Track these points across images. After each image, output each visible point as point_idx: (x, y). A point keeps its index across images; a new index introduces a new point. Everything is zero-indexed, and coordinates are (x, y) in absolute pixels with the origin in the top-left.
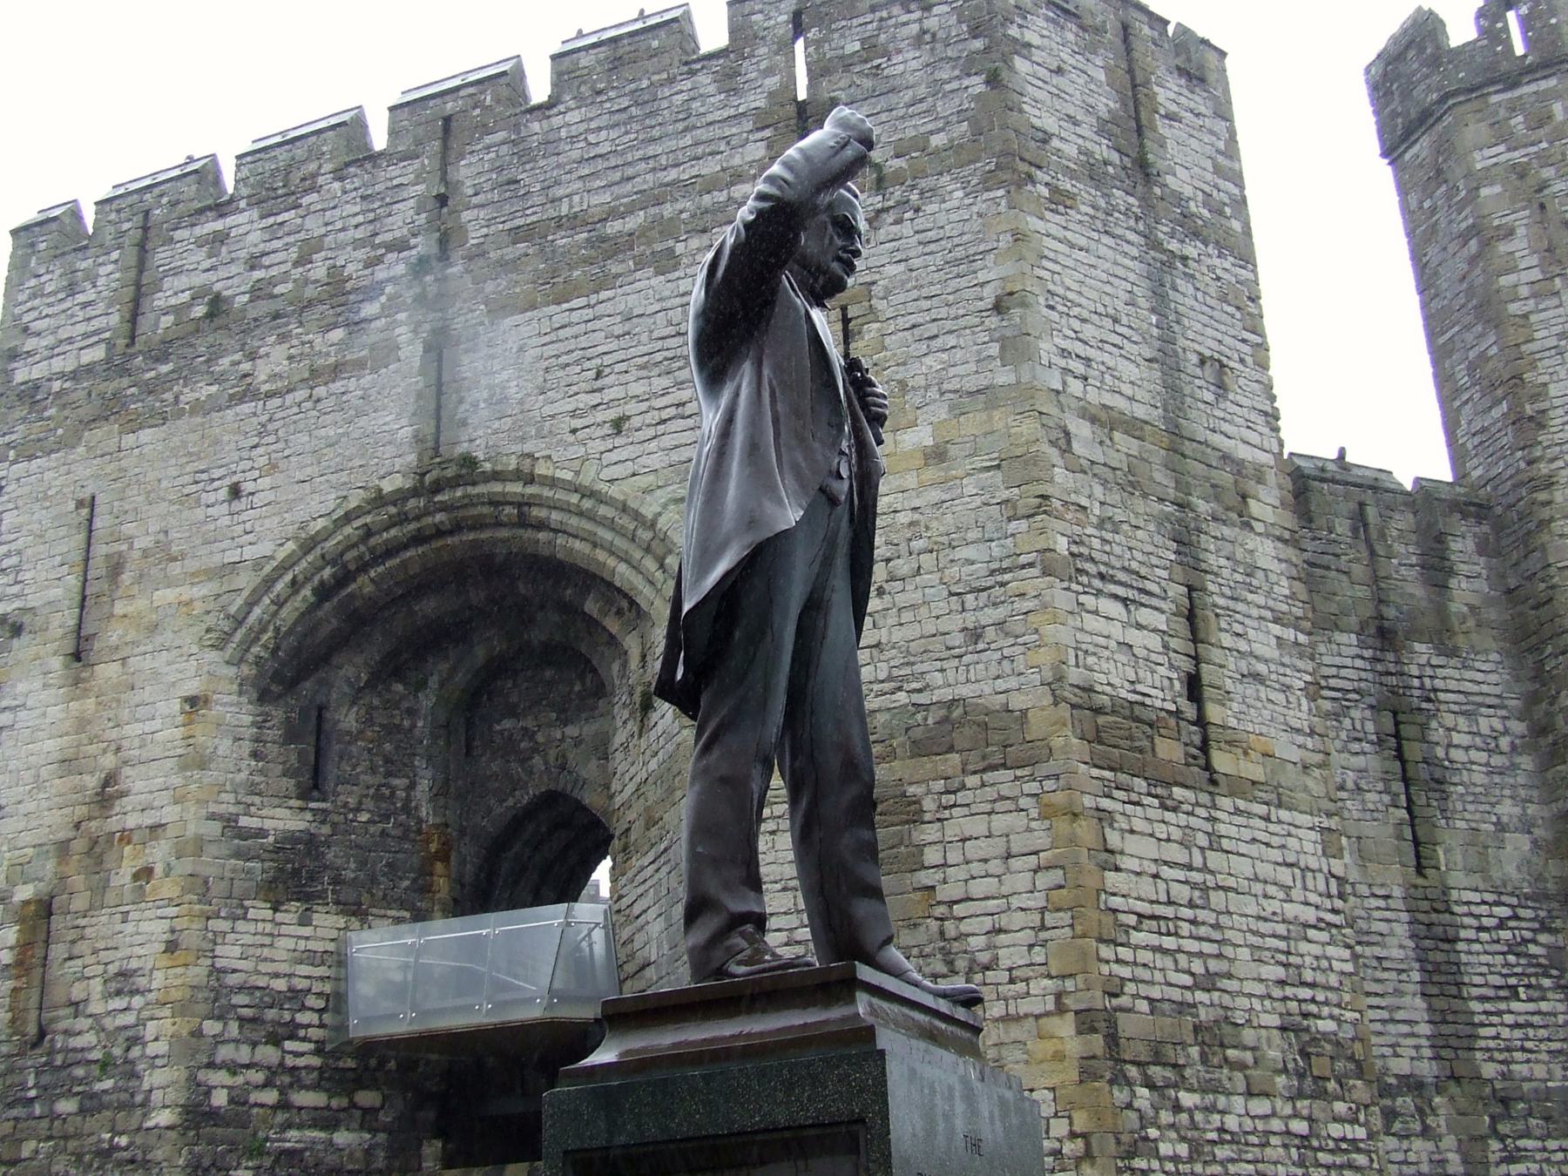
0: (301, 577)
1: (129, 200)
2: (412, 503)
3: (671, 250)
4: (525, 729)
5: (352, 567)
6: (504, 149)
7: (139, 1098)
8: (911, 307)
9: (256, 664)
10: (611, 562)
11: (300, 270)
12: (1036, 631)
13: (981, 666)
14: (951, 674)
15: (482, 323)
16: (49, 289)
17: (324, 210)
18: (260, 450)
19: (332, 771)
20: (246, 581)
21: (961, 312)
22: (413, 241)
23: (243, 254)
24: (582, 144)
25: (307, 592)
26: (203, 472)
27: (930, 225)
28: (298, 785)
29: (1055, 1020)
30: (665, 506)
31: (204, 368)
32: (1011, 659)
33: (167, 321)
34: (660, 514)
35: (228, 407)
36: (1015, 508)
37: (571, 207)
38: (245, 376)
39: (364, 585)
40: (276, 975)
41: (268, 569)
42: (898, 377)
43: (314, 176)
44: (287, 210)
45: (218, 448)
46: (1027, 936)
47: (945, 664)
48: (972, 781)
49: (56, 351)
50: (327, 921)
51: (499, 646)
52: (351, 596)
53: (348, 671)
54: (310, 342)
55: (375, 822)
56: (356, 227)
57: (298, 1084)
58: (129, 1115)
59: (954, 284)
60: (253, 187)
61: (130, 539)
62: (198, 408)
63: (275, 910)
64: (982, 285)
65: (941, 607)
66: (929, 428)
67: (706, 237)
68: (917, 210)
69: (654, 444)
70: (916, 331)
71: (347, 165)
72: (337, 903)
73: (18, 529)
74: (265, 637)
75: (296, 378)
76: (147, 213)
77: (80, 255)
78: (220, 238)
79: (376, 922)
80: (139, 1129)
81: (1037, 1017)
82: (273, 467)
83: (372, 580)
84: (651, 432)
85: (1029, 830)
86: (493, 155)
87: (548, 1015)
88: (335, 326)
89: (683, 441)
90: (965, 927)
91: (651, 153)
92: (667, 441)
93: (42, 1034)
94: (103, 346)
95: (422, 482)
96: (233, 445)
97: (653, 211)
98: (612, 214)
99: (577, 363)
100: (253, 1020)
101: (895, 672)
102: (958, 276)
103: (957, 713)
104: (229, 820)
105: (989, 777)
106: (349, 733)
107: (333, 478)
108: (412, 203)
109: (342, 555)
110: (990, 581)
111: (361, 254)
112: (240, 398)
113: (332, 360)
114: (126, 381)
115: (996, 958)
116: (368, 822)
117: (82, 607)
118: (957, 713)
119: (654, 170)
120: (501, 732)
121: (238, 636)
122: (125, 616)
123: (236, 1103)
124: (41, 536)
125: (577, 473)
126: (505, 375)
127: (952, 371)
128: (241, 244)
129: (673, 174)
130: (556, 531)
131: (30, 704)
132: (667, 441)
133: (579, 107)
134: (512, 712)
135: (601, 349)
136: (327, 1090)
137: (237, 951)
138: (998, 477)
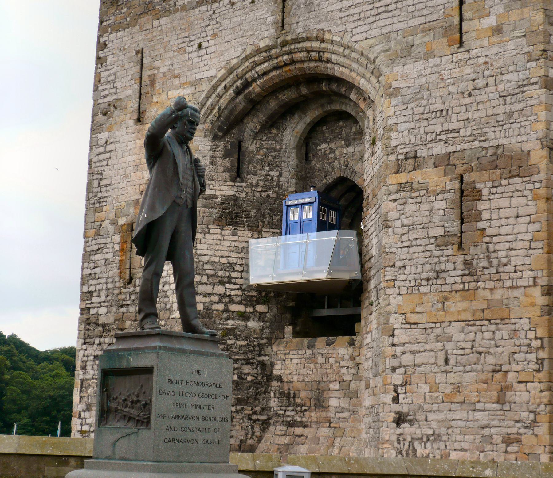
0: (228, 85)
2: (273, 51)
4: (331, 149)
7: (168, 306)
9: (211, 124)
10: (358, 78)
14: (498, 133)
19: (244, 169)
20: (205, 87)
25: (231, 91)
26: (187, 37)
28: (231, 176)
30: (379, 54)
32: (525, 127)
34: (377, 57)
35: (196, 7)
39: (255, 88)
40: (223, 257)
41: (214, 82)
46: (523, 252)
47: (496, 129)
48: (504, 182)
52: (250, 92)
53: (251, 125)
55: (264, 191)
57: (232, 302)
58: (165, 313)
61: (158, 68)
63: (222, 229)
65: (495, 103)
66: (495, 17)
69: (375, 24)
72: (248, 226)
74: (214, 111)
80: (169, 318)
81: (525, 287)
84: (373, 19)
85: (527, 205)
87: (329, 277)
89: (388, 23)
90: (497, 247)
92: (381, 23)
95: (276, 42)
96: (198, 26)
100: (213, 276)
101: (474, 132)
103: (500, 151)
105: (512, 181)
106: (253, 152)
107: (240, 40)
109: (245, 74)
110: (517, 91)
116: (261, 191)
117: (140, 98)
118: (500, 151)
120: (321, 150)
122: (157, 102)
125: (342, 38)
130: (335, 64)
132: (381, 23)
134: (325, 141)
136: (244, 305)
137: (206, 247)
138: (523, 41)
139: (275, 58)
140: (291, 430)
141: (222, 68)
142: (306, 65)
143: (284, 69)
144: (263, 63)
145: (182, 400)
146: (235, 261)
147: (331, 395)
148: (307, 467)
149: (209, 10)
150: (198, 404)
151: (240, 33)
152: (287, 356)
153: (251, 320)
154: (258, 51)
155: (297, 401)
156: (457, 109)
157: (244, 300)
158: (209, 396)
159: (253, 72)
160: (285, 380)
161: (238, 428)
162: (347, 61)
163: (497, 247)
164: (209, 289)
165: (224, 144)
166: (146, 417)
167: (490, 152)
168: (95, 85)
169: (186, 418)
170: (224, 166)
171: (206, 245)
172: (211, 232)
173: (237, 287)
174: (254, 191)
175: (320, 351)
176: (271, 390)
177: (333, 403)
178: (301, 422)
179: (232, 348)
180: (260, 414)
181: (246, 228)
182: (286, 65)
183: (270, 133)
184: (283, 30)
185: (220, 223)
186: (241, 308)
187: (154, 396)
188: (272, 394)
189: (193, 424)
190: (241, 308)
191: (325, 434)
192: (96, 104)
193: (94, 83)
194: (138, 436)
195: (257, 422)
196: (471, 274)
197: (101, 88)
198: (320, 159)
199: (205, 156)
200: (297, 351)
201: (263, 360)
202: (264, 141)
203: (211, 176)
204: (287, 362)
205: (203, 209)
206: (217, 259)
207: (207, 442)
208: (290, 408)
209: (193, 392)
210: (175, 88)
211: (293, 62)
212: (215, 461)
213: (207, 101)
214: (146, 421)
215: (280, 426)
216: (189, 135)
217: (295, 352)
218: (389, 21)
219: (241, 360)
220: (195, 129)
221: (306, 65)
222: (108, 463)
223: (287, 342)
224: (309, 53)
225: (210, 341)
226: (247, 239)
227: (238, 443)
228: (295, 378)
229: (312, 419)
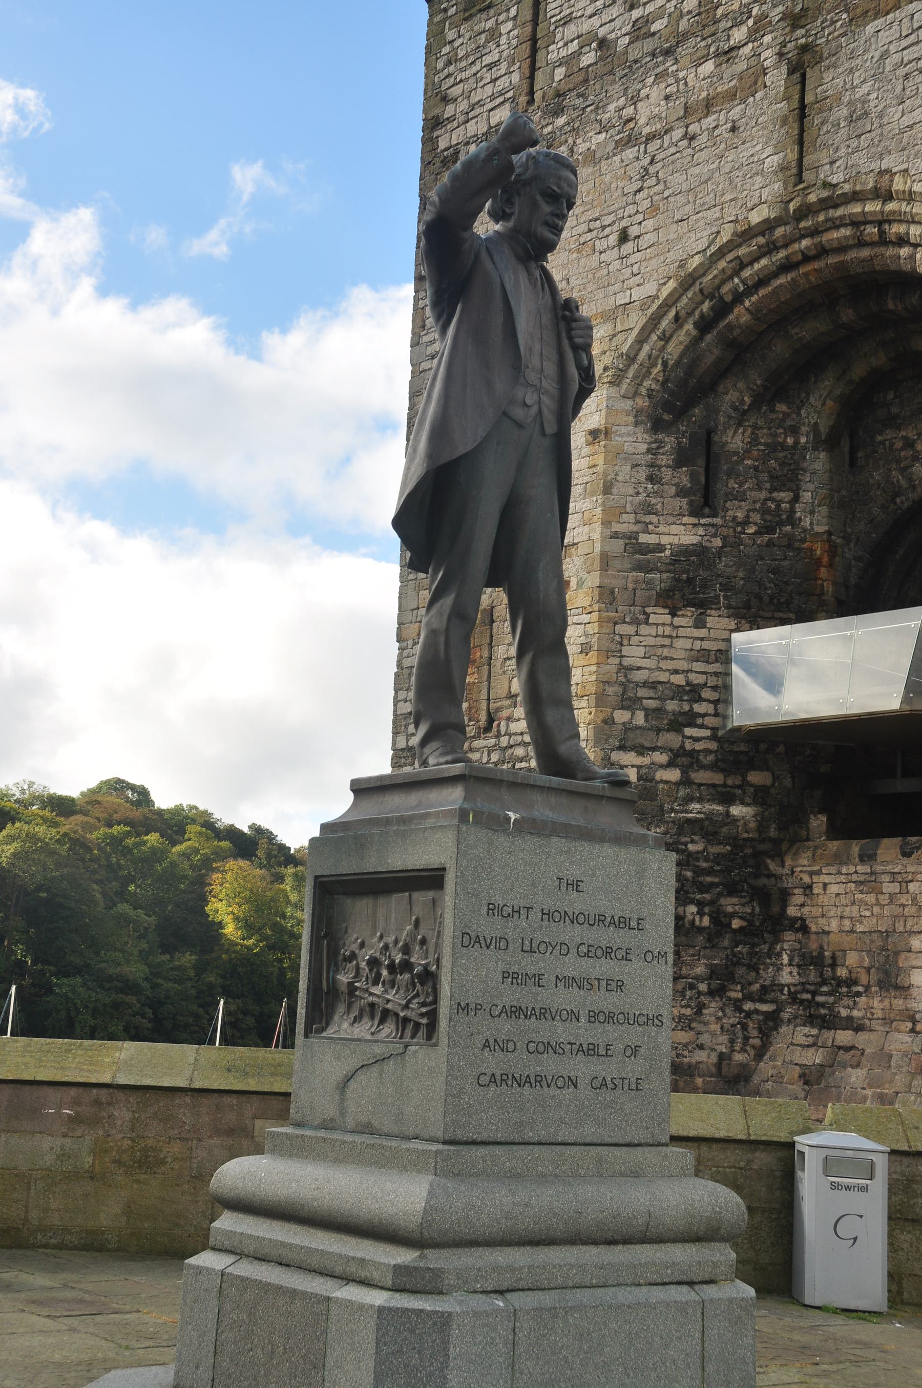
0: (683, 313)
2: (779, 231)
5: (728, 298)
9: (649, 396)
16: (461, 53)
20: (636, 321)
25: (689, 326)
26: (596, 220)
28: (691, 504)
31: (593, 116)
33: (560, 73)
35: (614, 155)
39: (740, 315)
40: (676, 672)
41: (655, 307)
49: (471, 115)
50: (717, 621)
51: (880, 360)
52: (729, 325)
53: (732, 396)
63: (673, 615)
72: (728, 607)
74: (655, 371)
77: (484, 16)
82: (654, 209)
83: (747, 309)
87: (907, 708)
88: (705, 58)
93: (491, 720)
95: (786, 210)
96: (620, 191)
100: (656, 710)
104: (630, 538)
106: (736, 453)
109: (719, 287)
116: (755, 533)
120: (882, 443)
121: (631, 373)
123: (646, 780)
126: (865, 89)
134: (893, 422)
137: (641, 651)
139: (782, 247)
140: (828, 1035)
141: (670, 278)
142: (852, 255)
143: (803, 270)
144: (757, 259)
145: (528, 964)
146: (701, 679)
147: (914, 963)
148: (876, 1137)
149: (641, 156)
150: (575, 974)
151: (707, 199)
152: (815, 879)
153: (738, 802)
154: (746, 235)
155: (839, 974)
157: (723, 761)
158: (608, 952)
159: (736, 280)
160: (814, 928)
161: (715, 1027)
165: (677, 438)
166: (424, 1010)
168: (413, 333)
169: (544, 1013)
170: (677, 485)
171: (642, 648)
172: (650, 621)
173: (708, 733)
174: (740, 533)
175: (889, 868)
176: (782, 949)
178: (850, 1018)
179: (698, 860)
180: (762, 1001)
181: (724, 611)
182: (806, 258)
183: (773, 411)
184: (801, 181)
185: (669, 602)
187: (447, 951)
188: (785, 958)
189: (561, 1032)
191: (903, 1047)
193: (413, 329)
194: (404, 1066)
195: (755, 1016)
197: (425, 339)
198: (881, 463)
199: (637, 465)
200: (836, 867)
201: (765, 886)
202: (762, 428)
203: (649, 505)
204: (816, 891)
205: (634, 573)
206: (663, 677)
207: (604, 1084)
208: (825, 989)
209: (562, 938)
211: (823, 251)
212: (628, 1139)
213: (640, 349)
214: (424, 1021)
215: (804, 1025)
216: (548, 235)
217: (833, 870)
219: (717, 885)
220: (564, 217)
221: (852, 255)
222: (325, 1140)
223: (816, 848)
224: (858, 228)
225: (610, 799)
226: (725, 635)
227: (714, 1058)
228: (834, 925)
229: (872, 1014)
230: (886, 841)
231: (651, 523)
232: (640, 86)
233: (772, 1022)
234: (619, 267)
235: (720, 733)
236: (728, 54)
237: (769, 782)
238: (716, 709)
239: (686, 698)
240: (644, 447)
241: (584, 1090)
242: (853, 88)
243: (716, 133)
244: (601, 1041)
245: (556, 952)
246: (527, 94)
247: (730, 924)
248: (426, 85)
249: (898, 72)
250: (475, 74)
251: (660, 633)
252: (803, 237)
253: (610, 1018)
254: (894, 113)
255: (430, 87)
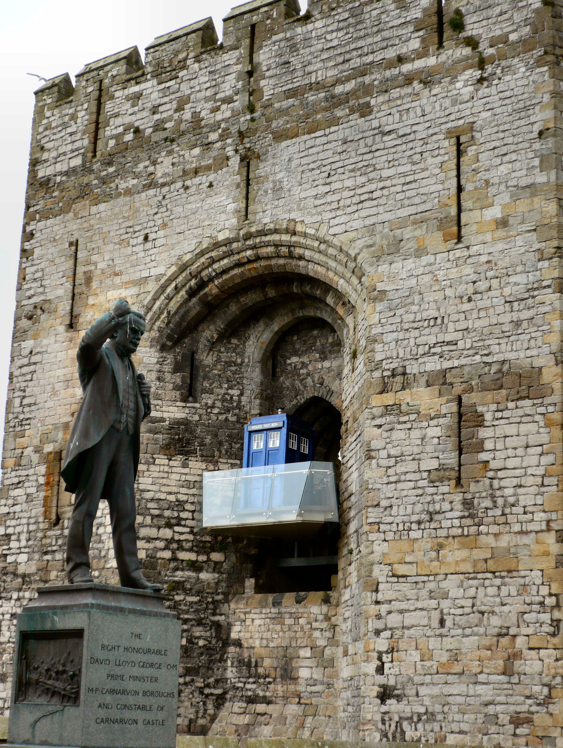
0: (179, 285)
1: (92, 74)
2: (235, 245)
3: (368, 104)
4: (303, 363)
5: (206, 279)
6: (283, 44)
7: (103, 553)
8: (494, 137)
10: (336, 278)
11: (178, 114)
12: (549, 324)
13: (519, 343)
14: (503, 346)
15: (270, 145)
16: (54, 125)
17: (190, 80)
18: (158, 216)
20: (152, 287)
21: (521, 140)
22: (235, 98)
23: (149, 105)
24: (323, 40)
25: (183, 293)
26: (130, 227)
27: (506, 88)
28: (182, 394)
29: (545, 534)
30: (361, 250)
32: (535, 339)
33: (112, 143)
34: (359, 254)
35: (143, 192)
36: (542, 254)
37: (316, 78)
38: (152, 174)
39: (212, 289)
40: (170, 493)
41: (163, 281)
42: (484, 178)
43: (185, 59)
44: (171, 80)
45: (138, 214)
46: (534, 490)
47: (501, 341)
48: (511, 405)
50: (196, 464)
52: (206, 294)
54: (183, 155)
55: (222, 414)
56: (206, 89)
59: (517, 123)
60: (154, 66)
61: (95, 264)
62: (128, 192)
63: (170, 460)
64: (532, 124)
66: (500, 207)
67: (387, 95)
68: (500, 79)
69: (356, 214)
70: (496, 151)
71: (202, 53)
72: (202, 456)
73: (41, 258)
74: (163, 317)
75: (176, 176)
76: (101, 81)
77: (68, 106)
78: (138, 96)
79: (221, 466)
80: (104, 568)
81: (537, 532)
84: (355, 208)
85: (538, 433)
86: (277, 47)
87: (300, 519)
88: (195, 146)
89: (372, 213)
91: (360, 46)
92: (364, 213)
94: (80, 157)
95: (238, 234)
96: (145, 213)
97: (360, 80)
98: (339, 81)
99: (318, 168)
100: (158, 516)
101: (475, 344)
102: (519, 119)
103: (505, 368)
106: (208, 366)
107: (195, 231)
108: (234, 75)
109: (200, 272)
110: (526, 295)
111: (209, 105)
112: (149, 186)
113: (194, 165)
114: (92, 176)
115: (518, 500)
117: (73, 299)
118: (505, 368)
119: (360, 56)
120: (290, 364)
122: (93, 305)
123: (151, 557)
124: (53, 261)
125: (317, 230)
127: (514, 175)
128: (148, 99)
129: (370, 58)
130: (308, 261)
131: (49, 350)
132: (364, 213)
133: (322, 18)
134: (296, 353)
135: (331, 160)
136: (196, 552)
137: (150, 481)
140: (252, 707)
141: (173, 265)
142: (273, 262)
143: (247, 267)
144: (222, 259)
145: (118, 671)
146: (185, 498)
147: (301, 664)
149: (158, 194)
151: (195, 223)
152: (247, 616)
154: (217, 245)
155: (259, 671)
156: (454, 317)
157: (196, 546)
158: (152, 665)
160: (245, 645)
161: (187, 704)
162: (323, 258)
163: (503, 483)
164: (153, 532)
166: (73, 691)
167: (494, 368)
168: (18, 283)
169: (124, 692)
170: (174, 383)
173: (188, 530)
174: (210, 413)
175: (289, 610)
177: (304, 673)
178: (265, 697)
180: (214, 688)
182: (249, 261)
183: (230, 343)
185: (167, 452)
186: (192, 556)
187: (84, 665)
188: (229, 663)
189: (131, 700)
190: (192, 556)
191: (294, 712)
192: (19, 306)
193: (18, 280)
194: (63, 715)
196: (471, 516)
198: (290, 375)
199: (151, 371)
201: (219, 621)
203: (157, 394)
205: (147, 434)
206: (163, 496)
207: (149, 723)
208: (251, 680)
209: (132, 660)
210: (115, 287)
211: (258, 258)
214: (73, 696)
215: (239, 702)
216: (132, 346)
217: (258, 611)
218: (374, 211)
219: (191, 620)
221: (273, 262)
223: (248, 598)
224: (277, 248)
226: (200, 472)
227: (186, 722)
228: (257, 643)
229: (277, 694)
230: (287, 595)
231: (158, 405)
232: (157, 156)
233: (220, 701)
234: (143, 255)
235: (195, 530)
236: (208, 146)
237: (222, 559)
238: (193, 516)
239: (175, 509)
240: (155, 360)
241: (140, 725)
242: (276, 174)
243: (200, 187)
244: (148, 704)
245: (130, 665)
246: (92, 152)
247: (197, 644)
248: (32, 140)
249: (298, 169)
250: (62, 137)
251: (161, 470)
252: (247, 249)
253: (152, 694)
254: (296, 190)
255: (34, 141)
